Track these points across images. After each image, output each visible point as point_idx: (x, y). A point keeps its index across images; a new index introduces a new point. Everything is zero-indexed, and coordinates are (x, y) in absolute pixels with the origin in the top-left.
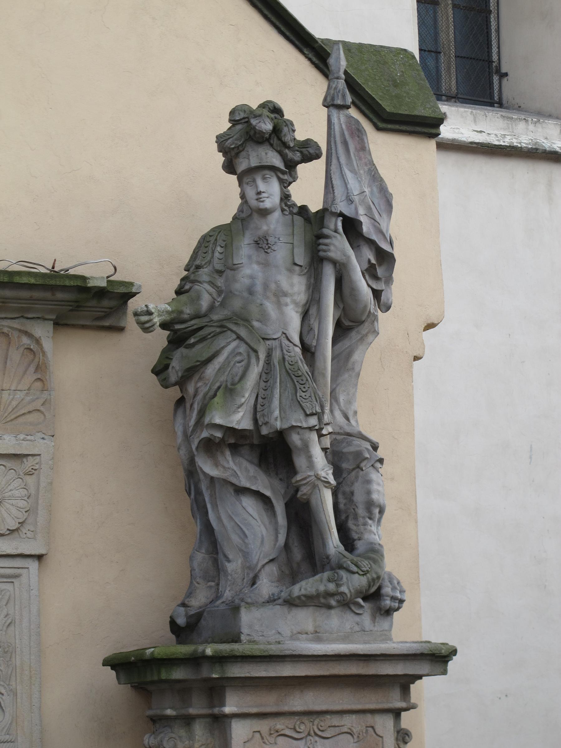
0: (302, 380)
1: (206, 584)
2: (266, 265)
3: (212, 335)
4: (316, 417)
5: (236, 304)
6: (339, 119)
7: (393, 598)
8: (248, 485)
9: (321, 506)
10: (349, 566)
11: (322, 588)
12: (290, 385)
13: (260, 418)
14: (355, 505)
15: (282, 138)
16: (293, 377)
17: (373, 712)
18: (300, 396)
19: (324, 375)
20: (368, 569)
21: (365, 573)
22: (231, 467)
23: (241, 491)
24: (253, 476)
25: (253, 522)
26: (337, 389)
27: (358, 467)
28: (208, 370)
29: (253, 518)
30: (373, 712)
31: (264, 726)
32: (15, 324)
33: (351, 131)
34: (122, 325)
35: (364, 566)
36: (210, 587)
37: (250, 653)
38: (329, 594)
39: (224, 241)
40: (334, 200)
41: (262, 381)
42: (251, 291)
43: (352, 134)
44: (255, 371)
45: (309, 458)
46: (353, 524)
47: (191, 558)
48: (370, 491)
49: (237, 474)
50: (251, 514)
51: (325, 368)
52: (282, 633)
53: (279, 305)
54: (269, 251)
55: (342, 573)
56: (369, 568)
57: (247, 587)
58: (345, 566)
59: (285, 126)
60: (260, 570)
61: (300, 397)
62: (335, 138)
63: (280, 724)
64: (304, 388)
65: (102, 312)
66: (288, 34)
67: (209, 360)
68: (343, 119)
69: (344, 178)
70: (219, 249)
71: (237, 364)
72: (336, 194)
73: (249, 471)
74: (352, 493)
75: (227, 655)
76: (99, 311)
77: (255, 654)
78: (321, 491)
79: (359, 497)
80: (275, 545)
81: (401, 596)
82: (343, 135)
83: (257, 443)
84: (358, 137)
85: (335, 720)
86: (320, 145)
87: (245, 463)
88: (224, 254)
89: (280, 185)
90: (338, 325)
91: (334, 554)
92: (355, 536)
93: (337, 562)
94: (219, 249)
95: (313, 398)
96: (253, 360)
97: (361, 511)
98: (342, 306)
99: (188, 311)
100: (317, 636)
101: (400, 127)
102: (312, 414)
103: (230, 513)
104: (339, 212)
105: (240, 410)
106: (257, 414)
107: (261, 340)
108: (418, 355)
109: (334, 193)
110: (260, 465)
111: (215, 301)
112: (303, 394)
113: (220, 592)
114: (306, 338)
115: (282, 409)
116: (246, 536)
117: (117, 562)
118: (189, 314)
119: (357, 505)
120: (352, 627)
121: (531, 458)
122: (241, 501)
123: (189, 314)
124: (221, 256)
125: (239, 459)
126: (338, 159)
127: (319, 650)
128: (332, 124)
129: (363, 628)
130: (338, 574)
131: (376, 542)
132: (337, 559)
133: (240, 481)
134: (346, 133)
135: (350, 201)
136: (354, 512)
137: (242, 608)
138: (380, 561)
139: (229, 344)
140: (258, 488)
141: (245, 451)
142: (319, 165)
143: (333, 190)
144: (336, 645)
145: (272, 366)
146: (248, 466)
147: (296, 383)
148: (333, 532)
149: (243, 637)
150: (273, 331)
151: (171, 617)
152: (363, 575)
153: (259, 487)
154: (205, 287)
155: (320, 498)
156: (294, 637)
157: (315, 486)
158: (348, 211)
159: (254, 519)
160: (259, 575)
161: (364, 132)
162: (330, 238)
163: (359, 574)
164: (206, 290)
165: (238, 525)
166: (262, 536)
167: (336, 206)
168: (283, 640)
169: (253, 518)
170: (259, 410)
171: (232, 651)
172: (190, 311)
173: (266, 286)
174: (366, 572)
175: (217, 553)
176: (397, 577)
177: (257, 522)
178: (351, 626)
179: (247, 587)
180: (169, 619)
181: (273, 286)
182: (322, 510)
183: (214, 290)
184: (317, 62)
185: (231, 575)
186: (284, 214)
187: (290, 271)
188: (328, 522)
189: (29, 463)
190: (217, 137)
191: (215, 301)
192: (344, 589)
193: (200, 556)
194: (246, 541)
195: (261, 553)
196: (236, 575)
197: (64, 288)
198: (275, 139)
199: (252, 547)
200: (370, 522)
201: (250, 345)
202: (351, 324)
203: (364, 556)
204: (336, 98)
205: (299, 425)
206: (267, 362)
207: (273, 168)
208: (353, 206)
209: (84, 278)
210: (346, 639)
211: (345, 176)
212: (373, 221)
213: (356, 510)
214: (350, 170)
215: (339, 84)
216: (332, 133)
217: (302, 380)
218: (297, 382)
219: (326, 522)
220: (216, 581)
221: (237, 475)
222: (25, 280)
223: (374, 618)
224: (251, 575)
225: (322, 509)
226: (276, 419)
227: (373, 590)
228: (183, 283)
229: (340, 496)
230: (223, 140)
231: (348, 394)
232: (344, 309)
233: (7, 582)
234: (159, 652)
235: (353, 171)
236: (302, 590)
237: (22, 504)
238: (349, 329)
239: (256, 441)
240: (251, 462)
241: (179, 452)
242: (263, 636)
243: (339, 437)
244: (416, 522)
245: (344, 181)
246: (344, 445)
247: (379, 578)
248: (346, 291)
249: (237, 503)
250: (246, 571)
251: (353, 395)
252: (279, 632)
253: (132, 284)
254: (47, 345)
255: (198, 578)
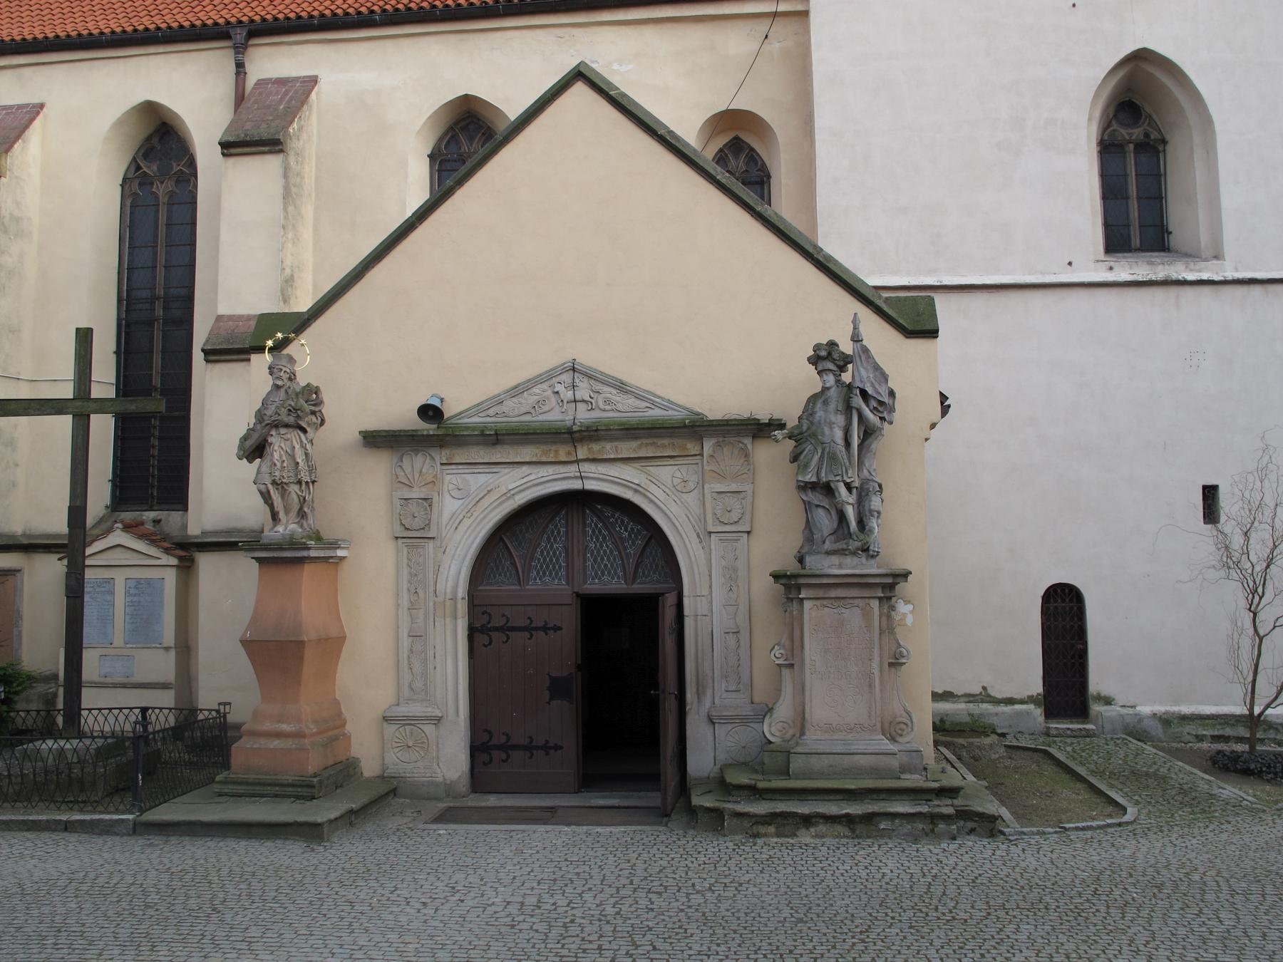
2: (826, 411)
5: (814, 428)
7: (874, 551)
11: (840, 547)
17: (869, 598)
23: (818, 506)
27: (867, 495)
30: (869, 598)
31: (818, 603)
32: (736, 439)
38: (843, 550)
42: (819, 423)
43: (863, 352)
44: (816, 457)
53: (831, 429)
63: (825, 602)
67: (801, 453)
79: (866, 508)
85: (851, 601)
87: (817, 495)
97: (867, 513)
100: (840, 567)
115: (826, 474)
141: (818, 489)
150: (826, 440)
156: (829, 567)
157: (843, 505)
158: (861, 386)
173: (825, 421)
181: (828, 420)
187: (836, 413)
189: (742, 495)
192: (850, 547)
197: (751, 424)
210: (853, 568)
222: (733, 423)
223: (867, 559)
233: (688, 551)
234: (796, 572)
235: (864, 368)
237: (739, 511)
240: (821, 494)
247: (867, 542)
253: (781, 420)
254: (750, 446)
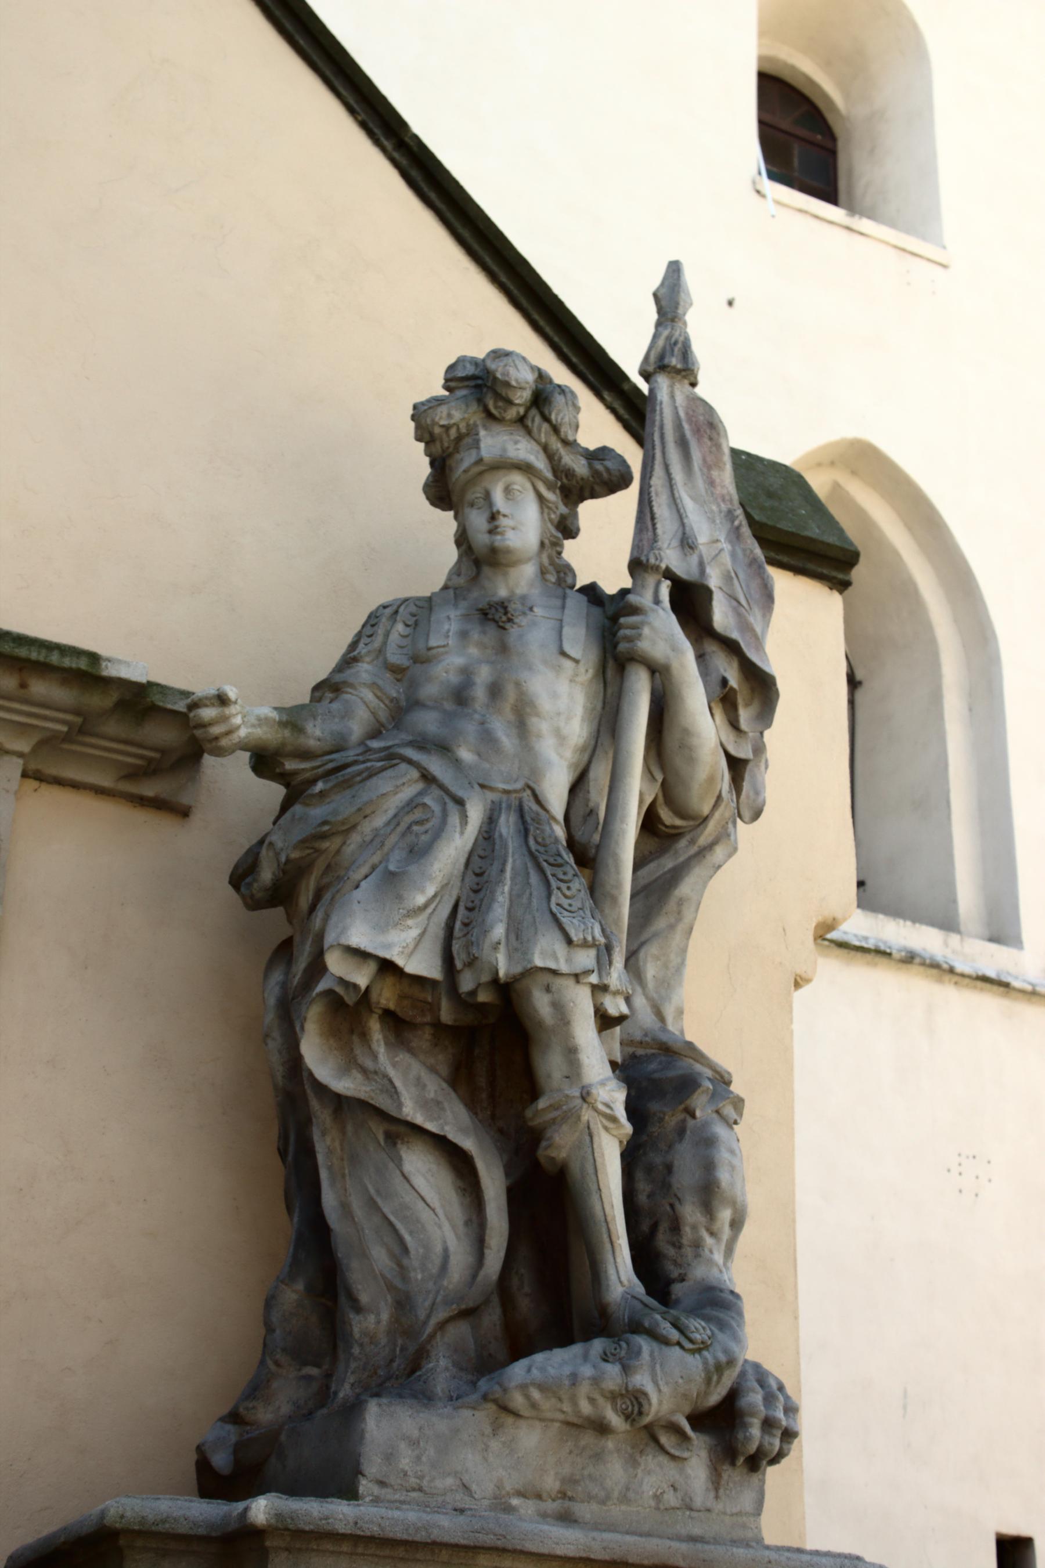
0: (569, 888)
1: (300, 1370)
3: (365, 775)
4: (592, 953)
6: (672, 397)
8: (419, 1119)
9: (593, 1177)
10: (657, 1324)
12: (534, 878)
13: (458, 954)
14: (675, 1195)
15: (550, 414)
16: (545, 864)
18: (558, 904)
19: (615, 900)
20: (706, 1338)
21: (700, 1348)
22: (382, 1068)
24: (432, 1099)
25: (426, 1215)
26: (642, 954)
28: (349, 845)
29: (428, 1205)
33: (696, 425)
34: (185, 800)
35: (696, 1328)
36: (308, 1378)
37: (375, 1530)
39: (414, 615)
40: (655, 539)
41: (470, 872)
43: (697, 431)
45: (571, 1052)
46: (668, 1242)
47: (270, 1303)
48: (713, 1163)
49: (395, 1087)
50: (423, 1194)
51: (619, 886)
52: (474, 1487)
54: (508, 626)
55: (644, 1343)
56: (709, 1338)
57: (397, 1379)
58: (647, 1324)
59: (560, 394)
60: (432, 1337)
61: (558, 907)
62: (662, 427)
64: (569, 888)
65: (135, 756)
66: (574, 360)
68: (680, 399)
69: (676, 505)
70: (400, 627)
71: (415, 828)
72: (659, 531)
73: (424, 1086)
74: (669, 1168)
75: (312, 1527)
76: (129, 754)
77: (391, 1535)
78: (596, 1139)
79: (685, 1176)
80: (474, 1276)
81: (787, 1420)
82: (679, 427)
83: (450, 1023)
84: (711, 439)
86: (630, 462)
87: (416, 1068)
88: (410, 638)
89: (542, 513)
90: (650, 823)
91: (618, 1299)
92: (675, 1273)
93: (626, 1320)
94: (400, 627)
95: (586, 912)
96: (454, 819)
98: (660, 777)
99: (318, 733)
101: (778, 555)
102: (585, 944)
103: (372, 1191)
104: (663, 566)
105: (410, 922)
106: (454, 942)
107: (476, 787)
108: (804, 975)
109: (654, 529)
110: (454, 1082)
111: (382, 729)
112: (565, 902)
113: (332, 1394)
114: (579, 830)
116: (405, 1250)
117: (101, 1321)
118: (319, 740)
119: (679, 1195)
120: (658, 1493)
121: (905, 1407)
122: (400, 1159)
123: (319, 740)
124: (405, 642)
125: (403, 1057)
126: (667, 467)
127: (569, 1544)
128: (658, 402)
129: (688, 1500)
130: (628, 1344)
131: (722, 1286)
132: (627, 1311)
133: (400, 1105)
134: (686, 426)
135: (687, 543)
136: (671, 1213)
137: (369, 1404)
138: (734, 1324)
139: (397, 790)
140: (442, 1129)
142: (627, 500)
143: (654, 525)
144: (616, 1534)
145: (498, 841)
146: (423, 1074)
147: (550, 877)
148: (620, 1245)
149: (365, 1486)
151: (199, 1449)
152: (693, 1352)
153: (447, 1128)
154: (362, 695)
155: (591, 1157)
159: (427, 1208)
160: (429, 1347)
161: (722, 433)
162: (643, 614)
163: (682, 1347)
164: (365, 703)
165: (391, 1224)
166: (446, 1250)
167: (659, 554)
168: (472, 1507)
169: (428, 1205)
170: (457, 936)
171: (327, 1518)
172: (323, 733)
173: (495, 691)
174: (702, 1346)
175: (334, 1298)
176: (776, 1374)
177: (435, 1217)
178: (657, 1490)
179: (397, 1379)
180: (194, 1457)
182: (594, 1187)
183: (382, 705)
184: (626, 416)
185: (361, 1345)
186: (545, 580)
188: (609, 1219)
190: (415, 407)
191: (382, 729)
193: (292, 1295)
194: (405, 1262)
195: (438, 1292)
196: (373, 1347)
198: (538, 419)
199: (419, 1277)
200: (709, 1240)
201: (448, 790)
202: (678, 822)
203: (695, 1311)
204: (668, 354)
205: (553, 965)
206: (486, 835)
207: (525, 468)
208: (694, 560)
209: (94, 658)
211: (678, 501)
212: (735, 603)
213: (677, 1206)
214: (691, 497)
215: (676, 330)
216: (658, 418)
217: (565, 874)
218: (553, 875)
219: (603, 1219)
220: (326, 1367)
221: (393, 1090)
224: (412, 1349)
225: (597, 1187)
226: (496, 946)
227: (715, 1398)
228: (317, 694)
229: (639, 1175)
230: (426, 407)
231: (666, 966)
232: (664, 784)
236: (535, 1371)
238: (673, 836)
239: (446, 1014)
241: (266, 1045)
242: (420, 1489)
243: (640, 1052)
244: (796, 1318)
245: (678, 511)
246: (652, 1066)
248: (671, 740)
249: (391, 1165)
250: (400, 1342)
251: (676, 971)
252: (464, 1486)
255: (279, 1350)
